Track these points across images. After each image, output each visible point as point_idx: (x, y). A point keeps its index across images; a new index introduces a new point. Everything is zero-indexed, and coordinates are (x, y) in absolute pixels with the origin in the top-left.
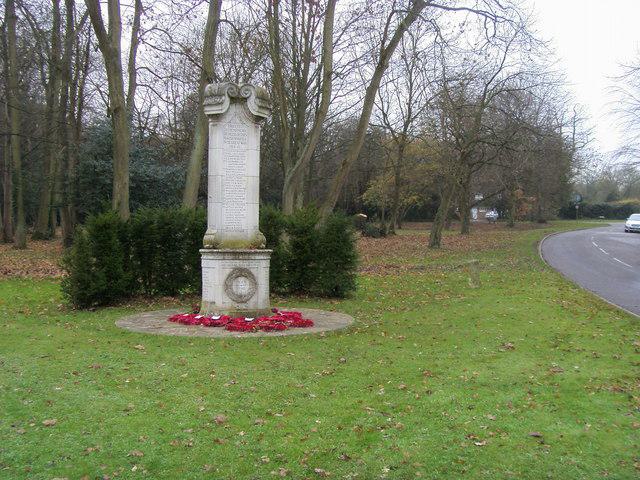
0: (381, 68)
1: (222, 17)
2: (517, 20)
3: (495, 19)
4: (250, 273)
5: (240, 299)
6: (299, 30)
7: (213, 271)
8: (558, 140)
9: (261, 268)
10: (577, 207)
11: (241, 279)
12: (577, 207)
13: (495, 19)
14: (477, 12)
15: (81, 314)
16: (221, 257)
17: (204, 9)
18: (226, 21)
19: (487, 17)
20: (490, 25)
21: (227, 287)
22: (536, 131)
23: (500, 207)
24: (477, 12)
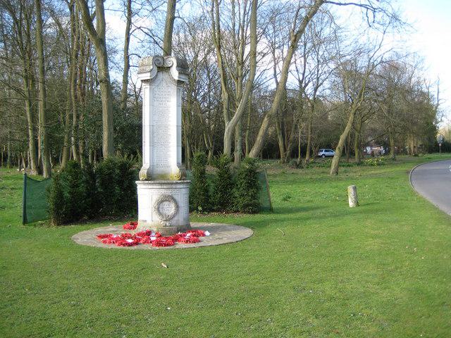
0: (294, 48)
1: (176, 15)
2: (390, 11)
3: (374, 10)
4: (173, 198)
5: (169, 219)
6: (237, 24)
7: (147, 196)
8: (425, 95)
9: (182, 195)
10: (440, 145)
11: (166, 203)
12: (440, 145)
13: (374, 10)
14: (361, 5)
15: (60, 227)
16: (160, 187)
17: (165, 7)
18: (179, 17)
19: (368, 8)
20: (370, 13)
21: (158, 208)
22: (410, 91)
23: (386, 145)
24: (361, 5)
